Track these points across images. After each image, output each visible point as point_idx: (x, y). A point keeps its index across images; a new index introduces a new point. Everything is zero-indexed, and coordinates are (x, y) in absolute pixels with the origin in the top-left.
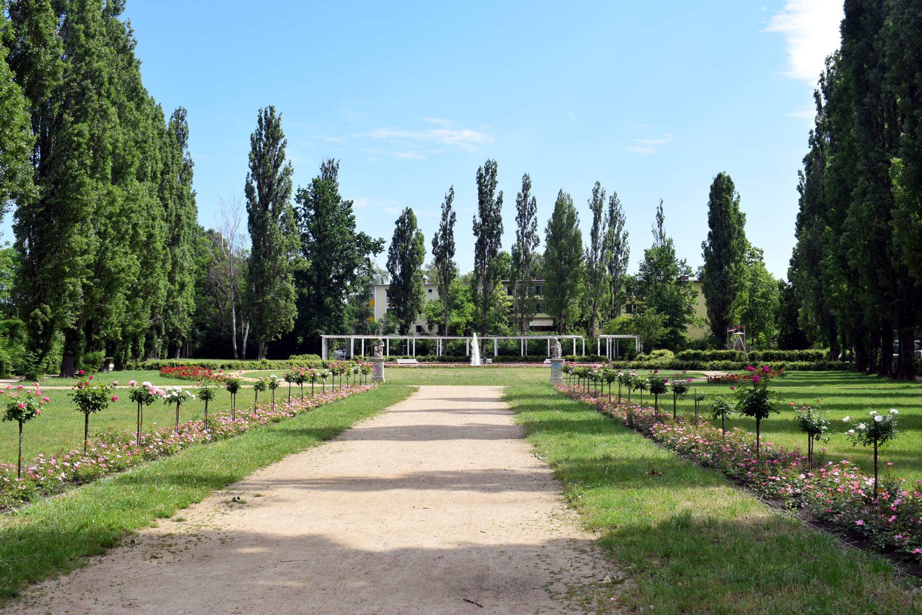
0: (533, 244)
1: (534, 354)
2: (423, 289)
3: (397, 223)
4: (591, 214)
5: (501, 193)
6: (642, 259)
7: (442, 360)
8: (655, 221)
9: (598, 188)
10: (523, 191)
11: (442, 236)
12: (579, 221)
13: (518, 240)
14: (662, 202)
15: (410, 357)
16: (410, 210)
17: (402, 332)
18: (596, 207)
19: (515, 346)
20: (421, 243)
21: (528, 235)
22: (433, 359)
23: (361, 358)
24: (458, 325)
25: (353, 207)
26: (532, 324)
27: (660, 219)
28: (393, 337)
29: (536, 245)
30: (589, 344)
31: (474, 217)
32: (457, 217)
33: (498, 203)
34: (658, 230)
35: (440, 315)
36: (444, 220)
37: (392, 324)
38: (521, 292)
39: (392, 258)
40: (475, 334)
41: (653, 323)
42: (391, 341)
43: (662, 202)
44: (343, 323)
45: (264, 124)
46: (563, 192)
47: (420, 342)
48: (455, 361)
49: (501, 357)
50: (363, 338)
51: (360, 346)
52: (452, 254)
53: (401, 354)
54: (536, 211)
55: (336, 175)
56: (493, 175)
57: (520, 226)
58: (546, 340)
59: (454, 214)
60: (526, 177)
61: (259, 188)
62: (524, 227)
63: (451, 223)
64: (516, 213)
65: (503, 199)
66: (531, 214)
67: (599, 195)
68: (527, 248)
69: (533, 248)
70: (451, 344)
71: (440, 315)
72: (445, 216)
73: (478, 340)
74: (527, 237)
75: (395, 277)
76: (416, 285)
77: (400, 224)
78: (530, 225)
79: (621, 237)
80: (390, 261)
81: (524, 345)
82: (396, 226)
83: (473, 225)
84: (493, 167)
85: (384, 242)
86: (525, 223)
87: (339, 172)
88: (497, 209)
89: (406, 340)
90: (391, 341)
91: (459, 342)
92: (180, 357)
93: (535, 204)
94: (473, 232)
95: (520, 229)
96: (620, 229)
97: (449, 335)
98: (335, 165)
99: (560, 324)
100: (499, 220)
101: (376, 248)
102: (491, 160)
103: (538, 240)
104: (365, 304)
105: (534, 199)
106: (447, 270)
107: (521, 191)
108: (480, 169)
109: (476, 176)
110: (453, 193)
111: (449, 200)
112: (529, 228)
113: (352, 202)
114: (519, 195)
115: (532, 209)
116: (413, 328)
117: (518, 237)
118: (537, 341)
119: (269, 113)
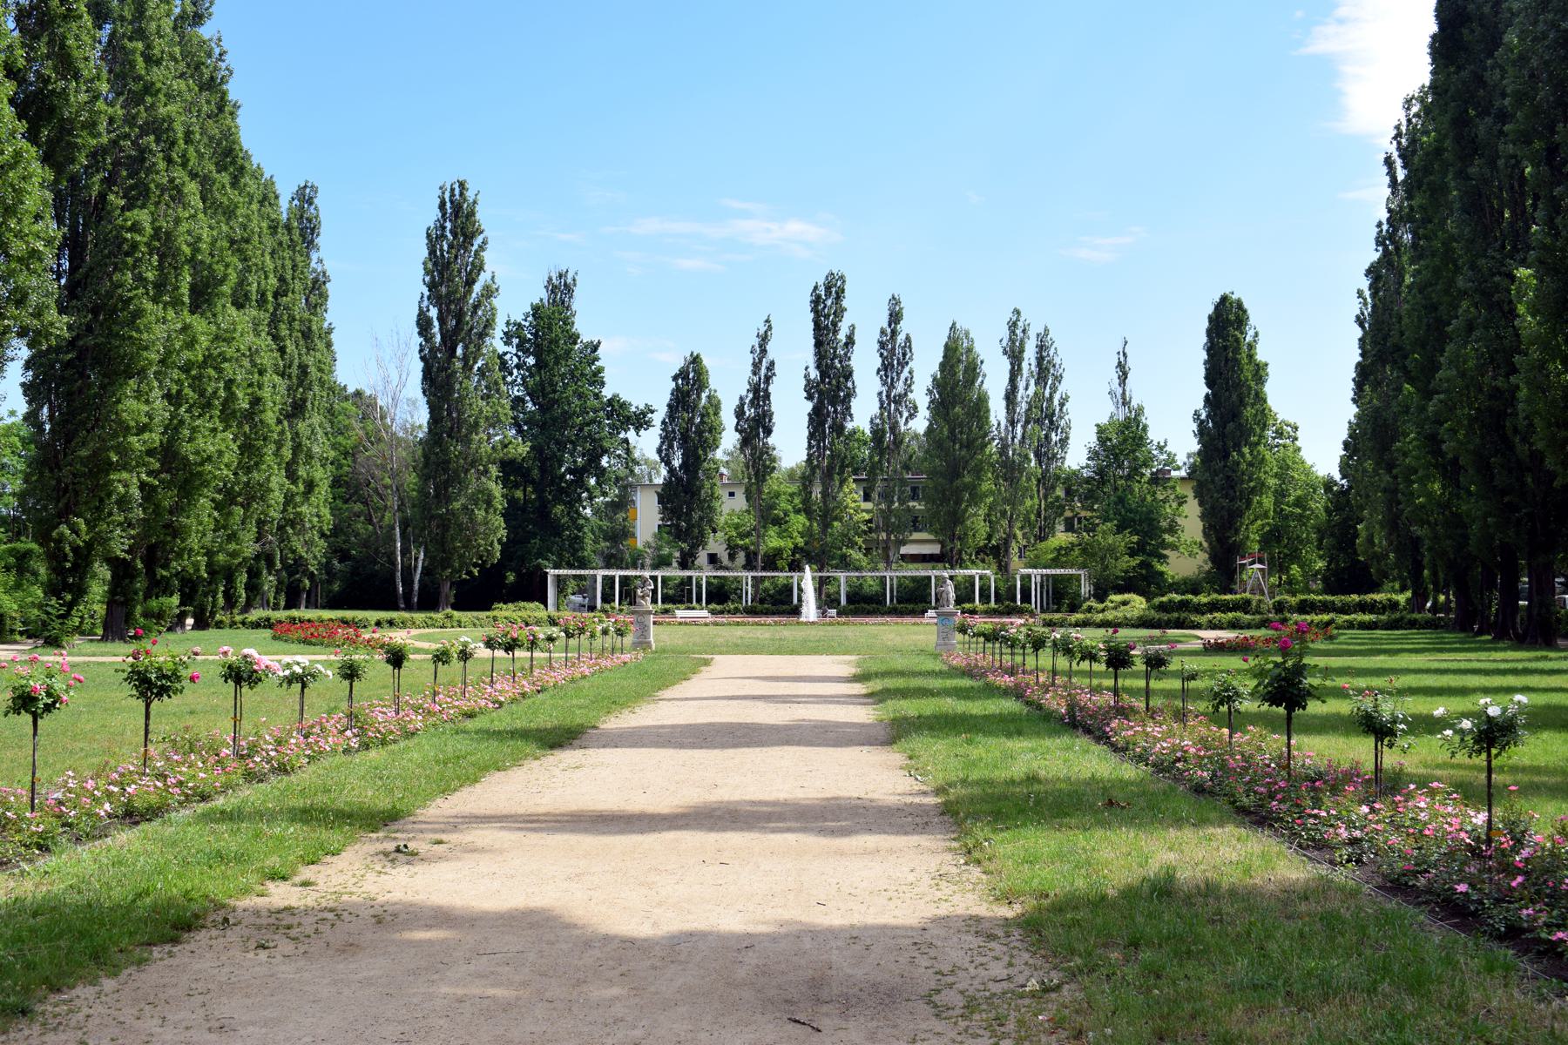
0: (906, 414)
1: (908, 601)
2: (719, 491)
3: (675, 378)
4: (1005, 364)
5: (853, 328)
6: (1092, 439)
7: (751, 612)
8: (1114, 376)
9: (1018, 320)
10: (890, 325)
11: (752, 402)
12: (984, 376)
13: (881, 407)
14: (1126, 343)
15: (697, 606)
16: (698, 356)
17: (684, 565)
18: (1013, 351)
19: (876, 588)
20: (716, 414)
21: (899, 400)
22: (736, 611)
23: (613, 608)
24: (778, 552)
25: (600, 351)
26: (904, 550)
27: (1123, 372)
28: (668, 572)
29: (912, 416)
30: (1001, 584)
31: (807, 368)
32: (777, 369)
33: (846, 344)
34: (1120, 391)
35: (748, 534)
36: (755, 373)
37: (666, 551)
38: (886, 496)
39: (667, 438)
40: (807, 567)
41: (1111, 550)
42: (664, 580)
43: (1126, 343)
44: (583, 549)
45: (449, 211)
46: (958, 326)
47: (715, 581)
48: (774, 613)
49: (852, 607)
50: (617, 574)
51: (613, 588)
52: (768, 432)
53: (681, 602)
54: (911, 358)
55: (571, 297)
56: (839, 298)
57: (884, 383)
58: (929, 578)
59: (772, 363)
60: (895, 301)
61: (441, 319)
62: (892, 386)
63: (768, 379)
64: (878, 362)
65: (856, 338)
66: (903, 364)
67: (1018, 332)
68: (897, 422)
69: (907, 422)
70: (767, 584)
71: (748, 534)
72: (756, 366)
73: (813, 578)
74: (895, 402)
75: (671, 471)
76: (707, 485)
77: (680, 381)
78: (901, 382)
79: (1056, 402)
80: (663, 443)
81: (892, 586)
82: (673, 385)
83: (804, 382)
84: (839, 283)
85: (652, 412)
86: (892, 379)
87: (577, 292)
88: (846, 354)
89: (690, 578)
90: (664, 580)
91: (781, 581)
92: (307, 607)
93: (910, 347)
94: (805, 394)
95: (884, 389)
96: (1054, 390)
97: (764, 569)
98: (569, 281)
99: (952, 550)
100: (848, 375)
101: (640, 421)
102: (835, 272)
103: (916, 408)
104: (620, 516)
105: (908, 339)
106: (760, 458)
107: (885, 325)
108: (816, 288)
109: (809, 299)
110: (770, 328)
111: (764, 339)
112: (900, 387)
113: (599, 342)
114: (883, 332)
115: (904, 355)
116: (702, 557)
117: (882, 403)
118: (914, 579)
119: (457, 192)
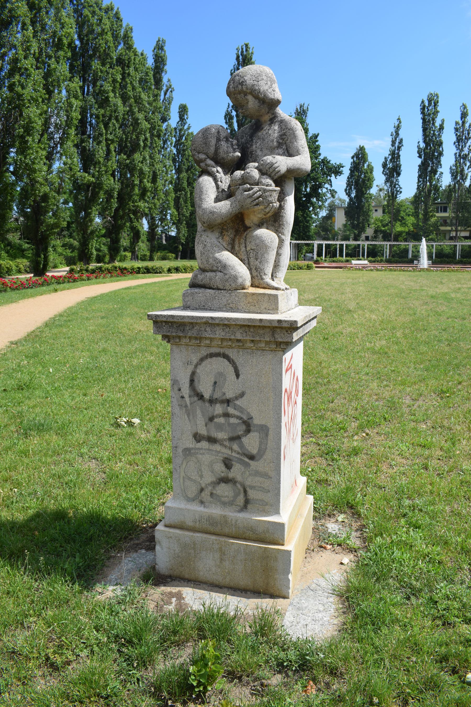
2: (371, 208)
3: (353, 157)
5: (443, 121)
7: (389, 261)
10: (461, 119)
11: (391, 160)
15: (362, 258)
16: (363, 147)
17: (356, 239)
20: (371, 172)
22: (381, 261)
23: (322, 259)
24: (400, 233)
25: (318, 139)
28: (348, 243)
31: (419, 142)
32: (404, 143)
33: (440, 129)
35: (387, 225)
36: (393, 146)
37: (348, 233)
39: (349, 184)
40: (424, 240)
42: (347, 246)
44: (309, 231)
45: (241, 60)
47: (371, 247)
48: (400, 262)
49: (439, 260)
50: (324, 243)
51: (322, 250)
52: (399, 174)
53: (355, 257)
55: (306, 116)
56: (436, 105)
57: (458, 149)
59: (401, 140)
61: (237, 116)
62: (462, 150)
63: (399, 148)
64: (454, 139)
65: (444, 125)
68: (463, 168)
70: (395, 248)
71: (387, 225)
72: (393, 143)
73: (427, 246)
74: (463, 158)
75: (351, 199)
76: (366, 205)
77: (355, 159)
80: (347, 187)
82: (352, 160)
83: (417, 149)
84: (435, 98)
85: (343, 167)
87: (309, 114)
88: (439, 135)
89: (359, 245)
90: (347, 246)
91: (403, 247)
92: (181, 259)
94: (418, 155)
97: (394, 241)
98: (305, 108)
100: (440, 144)
101: (337, 171)
102: (433, 93)
104: (329, 222)
106: (395, 187)
108: (423, 102)
109: (420, 108)
110: (400, 122)
111: (398, 128)
113: (318, 134)
114: (457, 123)
116: (363, 236)
117: (456, 158)
119: (244, 50)
